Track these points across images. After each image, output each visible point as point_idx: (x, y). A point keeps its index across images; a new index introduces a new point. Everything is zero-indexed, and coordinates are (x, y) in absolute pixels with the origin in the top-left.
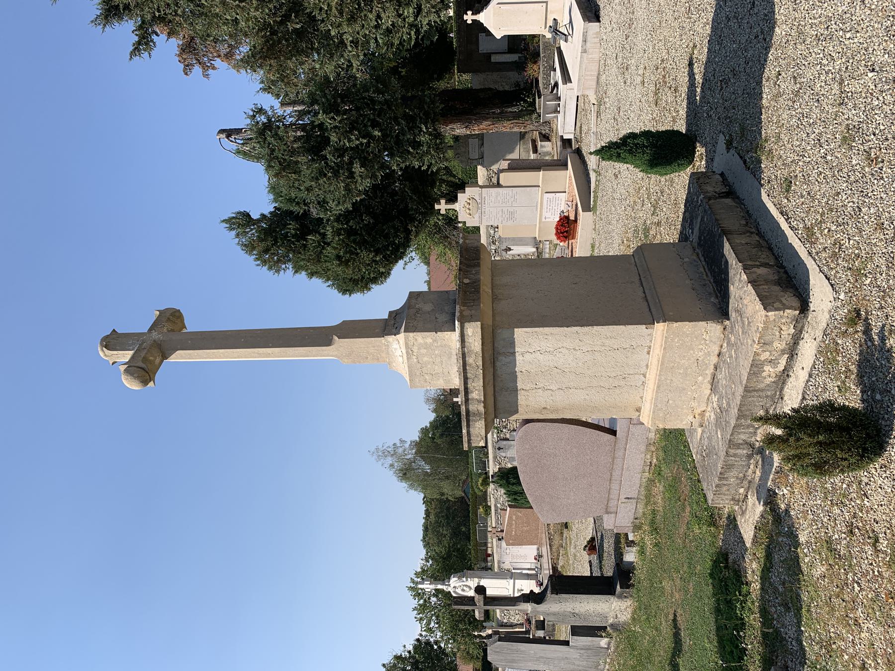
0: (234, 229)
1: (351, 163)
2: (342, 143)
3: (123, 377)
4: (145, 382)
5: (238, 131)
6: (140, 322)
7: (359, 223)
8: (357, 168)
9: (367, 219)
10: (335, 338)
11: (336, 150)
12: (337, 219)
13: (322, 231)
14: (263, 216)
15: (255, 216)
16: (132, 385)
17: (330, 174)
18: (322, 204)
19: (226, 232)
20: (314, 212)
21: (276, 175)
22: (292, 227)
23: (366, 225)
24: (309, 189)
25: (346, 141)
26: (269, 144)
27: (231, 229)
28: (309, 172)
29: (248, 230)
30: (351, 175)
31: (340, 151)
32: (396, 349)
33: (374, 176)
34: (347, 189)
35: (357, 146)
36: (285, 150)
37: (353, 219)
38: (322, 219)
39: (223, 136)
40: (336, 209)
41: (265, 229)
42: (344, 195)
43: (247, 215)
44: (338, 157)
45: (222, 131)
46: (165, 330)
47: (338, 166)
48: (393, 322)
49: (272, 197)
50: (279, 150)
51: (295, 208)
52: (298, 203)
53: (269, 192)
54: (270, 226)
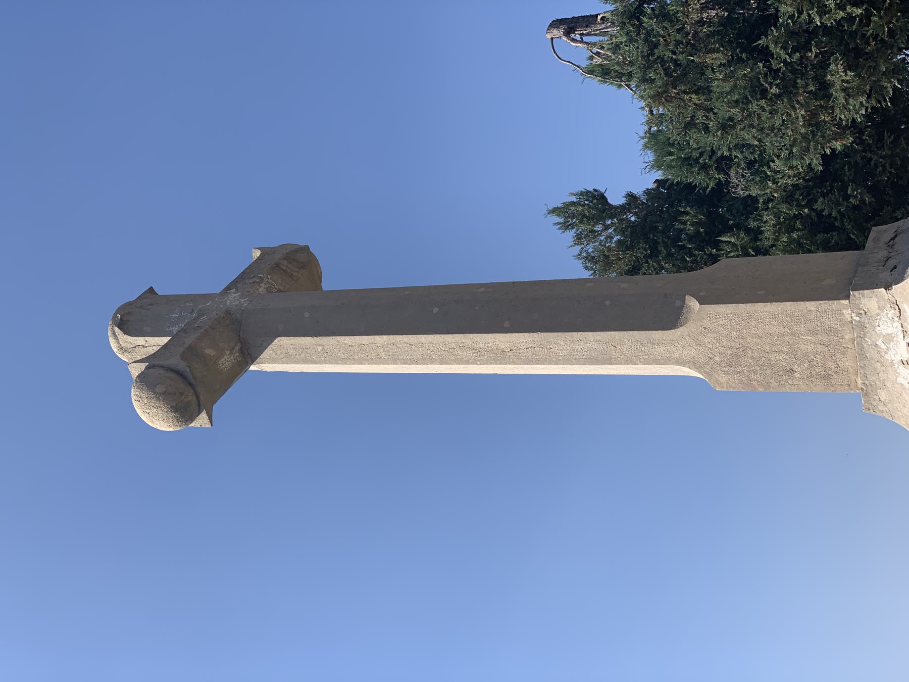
0: (572, 226)
1: (823, 65)
2: (804, 16)
3: (134, 392)
4: (184, 411)
5: (589, 20)
6: (204, 270)
7: (838, 204)
8: (839, 74)
9: (857, 194)
10: (693, 303)
11: (792, 34)
12: (789, 197)
13: (753, 224)
14: (631, 197)
15: (616, 199)
16: (155, 418)
17: (774, 90)
18: (757, 165)
19: (556, 232)
20: (741, 185)
21: (657, 98)
22: (690, 219)
23: (855, 207)
24: (727, 126)
25: (813, 13)
26: (649, 33)
27: (566, 226)
28: (727, 87)
29: (599, 228)
30: (824, 88)
31: (801, 37)
32: (888, 338)
33: (875, 91)
34: (813, 121)
35: (839, 23)
36: (678, 43)
37: (824, 195)
38: (754, 200)
39: (558, 32)
40: (787, 171)
41: (633, 225)
42: (804, 137)
43: (598, 198)
44: (795, 50)
45: (556, 24)
46: (262, 289)
47: (794, 71)
48: (883, 254)
49: (650, 156)
50: (667, 44)
51: (698, 179)
52: (705, 167)
53: (646, 147)
54: (645, 219)
